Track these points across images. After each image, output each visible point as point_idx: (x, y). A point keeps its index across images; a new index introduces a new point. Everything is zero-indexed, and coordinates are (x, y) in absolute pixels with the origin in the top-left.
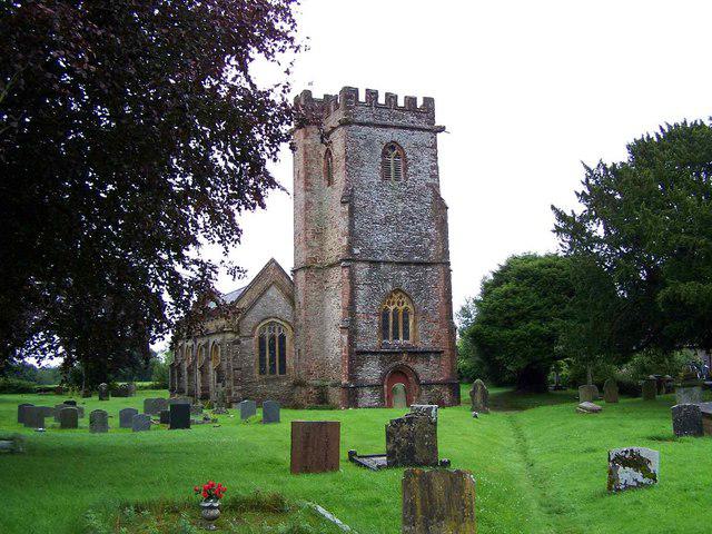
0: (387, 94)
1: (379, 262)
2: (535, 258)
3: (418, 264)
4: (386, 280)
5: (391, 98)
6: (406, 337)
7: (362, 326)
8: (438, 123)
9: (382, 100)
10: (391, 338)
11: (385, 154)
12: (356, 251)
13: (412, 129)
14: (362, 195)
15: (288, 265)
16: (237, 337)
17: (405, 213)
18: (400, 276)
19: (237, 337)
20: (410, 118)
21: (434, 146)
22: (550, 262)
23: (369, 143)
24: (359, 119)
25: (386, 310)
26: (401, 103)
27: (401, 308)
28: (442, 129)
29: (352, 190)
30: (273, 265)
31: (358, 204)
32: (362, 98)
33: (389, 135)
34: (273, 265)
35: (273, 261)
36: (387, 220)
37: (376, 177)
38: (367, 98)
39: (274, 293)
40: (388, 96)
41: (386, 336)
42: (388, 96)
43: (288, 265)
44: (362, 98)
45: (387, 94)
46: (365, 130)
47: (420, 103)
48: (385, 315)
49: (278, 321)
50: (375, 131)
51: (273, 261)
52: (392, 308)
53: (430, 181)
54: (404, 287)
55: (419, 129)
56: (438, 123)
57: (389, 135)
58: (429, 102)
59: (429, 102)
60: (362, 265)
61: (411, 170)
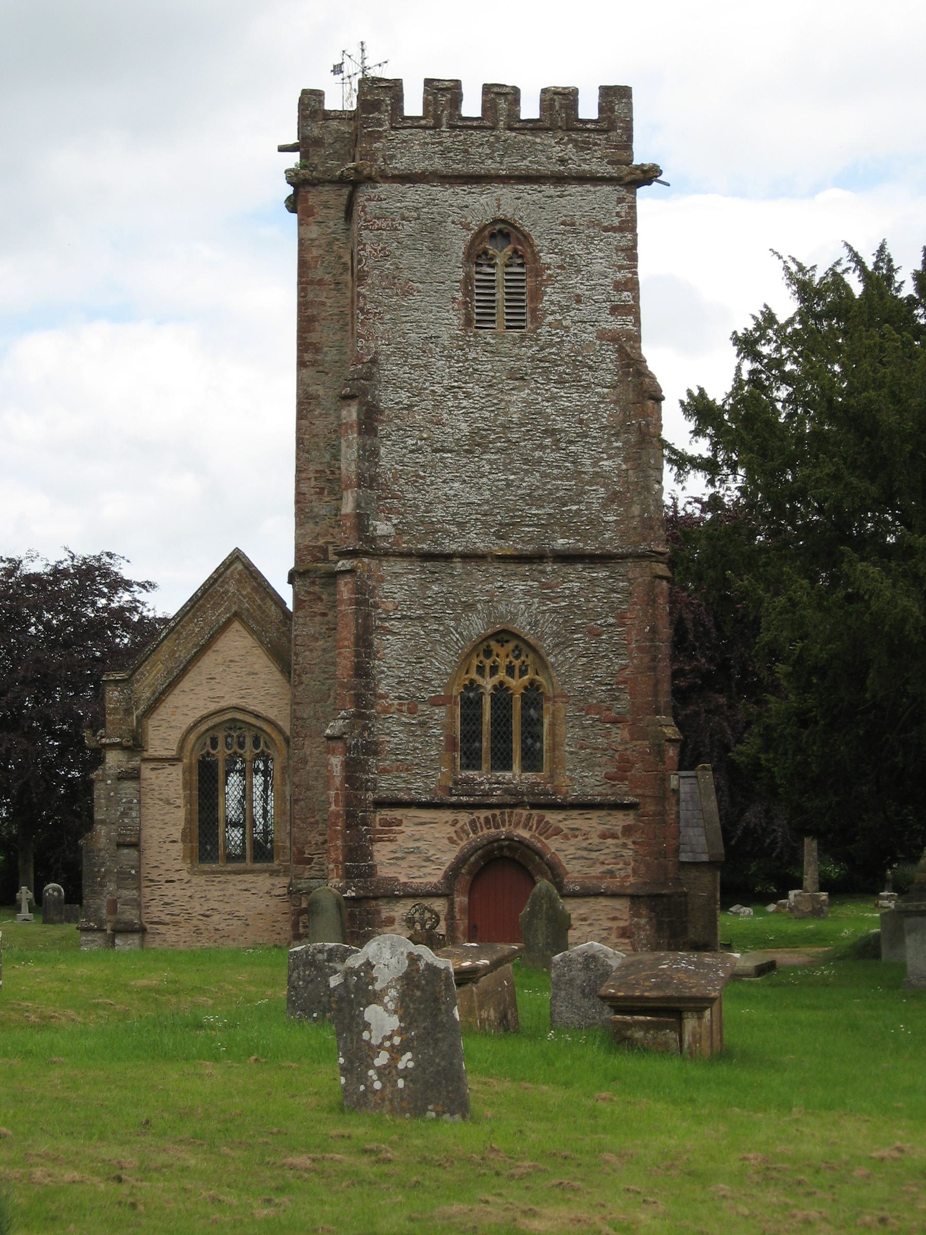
0: (488, 89)
1: (447, 557)
2: (661, 391)
3: (566, 558)
4: (469, 607)
5: (500, 97)
6: (532, 761)
7: (393, 733)
8: (641, 155)
9: (471, 107)
10: (486, 766)
11: (477, 255)
12: (382, 527)
13: (559, 180)
14: (403, 373)
15: (276, 564)
16: (135, 763)
17: (532, 416)
18: (508, 594)
19: (135, 763)
20: (553, 151)
21: (629, 225)
22: (853, 296)
23: (431, 229)
24: (401, 164)
25: (472, 686)
26: (530, 109)
27: (516, 684)
28: (649, 175)
29: (374, 361)
30: (237, 571)
31: (388, 398)
32: (413, 106)
33: (484, 204)
34: (237, 571)
35: (237, 557)
36: (477, 442)
37: (449, 322)
38: (426, 104)
39: (237, 643)
40: (492, 92)
41: (472, 760)
42: (492, 92)
43: (276, 564)
44: (413, 106)
45: (488, 89)
46: (414, 194)
47: (588, 109)
48: (471, 705)
49: (252, 720)
50: (444, 194)
51: (237, 557)
52: (488, 684)
53: (612, 324)
54: (522, 626)
55: (582, 179)
56: (641, 155)
57: (484, 204)
58: (615, 98)
59: (615, 98)
60: (399, 566)
61: (551, 295)
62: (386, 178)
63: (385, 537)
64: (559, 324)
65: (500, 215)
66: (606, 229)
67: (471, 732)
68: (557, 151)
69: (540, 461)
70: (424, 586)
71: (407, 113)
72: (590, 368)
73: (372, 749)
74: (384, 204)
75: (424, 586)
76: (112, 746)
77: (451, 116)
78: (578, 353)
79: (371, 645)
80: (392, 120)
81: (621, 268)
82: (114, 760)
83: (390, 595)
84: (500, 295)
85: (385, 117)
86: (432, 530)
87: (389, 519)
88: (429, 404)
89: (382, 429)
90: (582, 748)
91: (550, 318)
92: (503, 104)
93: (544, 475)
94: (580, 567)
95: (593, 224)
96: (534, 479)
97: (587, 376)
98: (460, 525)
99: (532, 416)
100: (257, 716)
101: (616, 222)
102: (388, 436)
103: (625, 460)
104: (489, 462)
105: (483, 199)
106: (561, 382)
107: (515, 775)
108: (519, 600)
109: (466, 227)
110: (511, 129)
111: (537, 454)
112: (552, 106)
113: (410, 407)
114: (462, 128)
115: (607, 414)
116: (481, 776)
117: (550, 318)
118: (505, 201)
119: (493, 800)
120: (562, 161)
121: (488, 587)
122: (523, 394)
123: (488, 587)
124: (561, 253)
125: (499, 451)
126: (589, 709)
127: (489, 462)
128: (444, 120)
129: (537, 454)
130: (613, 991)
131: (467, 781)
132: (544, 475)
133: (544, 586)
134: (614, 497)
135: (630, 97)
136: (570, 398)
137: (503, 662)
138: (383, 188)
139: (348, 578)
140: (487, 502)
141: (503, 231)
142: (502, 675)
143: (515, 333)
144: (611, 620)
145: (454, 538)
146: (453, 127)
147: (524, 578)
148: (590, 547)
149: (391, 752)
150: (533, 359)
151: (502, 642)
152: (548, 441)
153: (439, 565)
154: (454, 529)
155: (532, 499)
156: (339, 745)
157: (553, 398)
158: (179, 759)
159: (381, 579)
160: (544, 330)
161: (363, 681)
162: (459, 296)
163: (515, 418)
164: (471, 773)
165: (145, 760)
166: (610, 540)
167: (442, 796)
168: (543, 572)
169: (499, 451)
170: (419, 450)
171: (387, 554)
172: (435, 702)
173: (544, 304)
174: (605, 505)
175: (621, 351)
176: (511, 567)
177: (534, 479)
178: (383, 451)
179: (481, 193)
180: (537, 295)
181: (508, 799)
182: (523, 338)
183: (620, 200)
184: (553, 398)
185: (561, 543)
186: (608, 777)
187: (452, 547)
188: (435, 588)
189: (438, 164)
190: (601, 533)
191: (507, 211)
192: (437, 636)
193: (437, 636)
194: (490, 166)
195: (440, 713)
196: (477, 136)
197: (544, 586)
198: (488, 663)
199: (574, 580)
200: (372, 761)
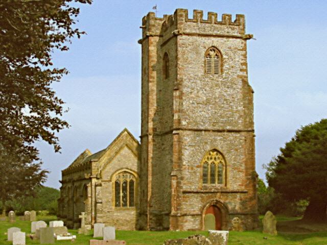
1: (201, 130)
3: (229, 131)
4: (206, 143)
10: (209, 182)
13: (228, 37)
14: (189, 84)
17: (221, 96)
18: (215, 140)
24: (188, 31)
36: (207, 102)
41: (205, 181)
46: (191, 38)
50: (199, 39)
52: (210, 162)
54: (219, 149)
60: (188, 132)
61: (226, 66)
62: (185, 34)
63: (185, 125)
64: (227, 73)
65: (213, 45)
66: (239, 50)
67: (205, 175)
68: (226, 30)
69: (223, 107)
70: (195, 138)
71: (189, 18)
72: (235, 84)
73: (182, 178)
74: (184, 41)
75: (195, 138)
76: (94, 178)
77: (200, 20)
78: (232, 80)
79: (182, 152)
80: (185, 19)
81: (242, 60)
82: (94, 181)
83: (186, 140)
84: (213, 65)
85: (184, 19)
86: (197, 124)
87: (185, 121)
88: (196, 92)
89: (184, 98)
90: (233, 178)
91: (226, 72)
92: (213, 17)
93: (224, 110)
94: (233, 133)
95: (236, 48)
96: (221, 112)
97: (235, 86)
98: (204, 123)
99: (221, 96)
100: (226, 178)
101: (241, 48)
102: (185, 100)
103: (244, 107)
104: (211, 107)
105: (209, 41)
106: (228, 88)
107: (217, 185)
108: (220, 142)
109: (205, 48)
110: (215, 23)
111: (222, 105)
112: (225, 19)
113: (191, 93)
114: (203, 23)
115: (240, 96)
116: (209, 185)
117: (226, 72)
118: (216, 42)
119: (212, 191)
120: (228, 32)
121: (211, 138)
122: (219, 90)
123: (211, 138)
124: (228, 55)
125: (214, 104)
126: (235, 169)
127: (211, 107)
128: (199, 21)
129: (222, 105)
130: (177, 231)
131: (205, 186)
132: (224, 110)
133: (224, 138)
134: (241, 116)
135: (244, 17)
136: (230, 91)
137: (213, 157)
138: (184, 37)
139: (177, 135)
140: (210, 117)
141: (214, 48)
142: (213, 160)
143: (217, 75)
144: (240, 147)
145: (202, 126)
146: (201, 22)
147: (220, 136)
148: (236, 128)
149: (187, 179)
150: (221, 81)
151: (213, 152)
152: (225, 102)
153: (199, 132)
154: (202, 124)
155: (221, 116)
156: (175, 178)
157: (226, 91)
158: (110, 181)
159: (184, 136)
160: (224, 74)
161: (180, 161)
162: (203, 65)
163: (217, 96)
164: (205, 184)
165: (102, 181)
166: (240, 127)
167: (199, 190)
168: (224, 135)
169: (214, 104)
170: (193, 103)
171: (185, 130)
172: (198, 167)
173: (224, 68)
174: (239, 118)
175: (243, 81)
176: (216, 133)
177: (221, 112)
178: (184, 103)
179: (208, 40)
180: (222, 65)
181: (216, 191)
182: (219, 76)
183: (242, 43)
184: (226, 91)
185: (228, 128)
186: (240, 185)
187: (202, 128)
188: (198, 138)
189: (198, 32)
190: (238, 125)
191: (215, 44)
192: (198, 150)
193: (198, 150)
194: (210, 33)
195: (199, 169)
196: (207, 25)
197: (224, 138)
198: (210, 157)
199: (232, 136)
200: (182, 181)
